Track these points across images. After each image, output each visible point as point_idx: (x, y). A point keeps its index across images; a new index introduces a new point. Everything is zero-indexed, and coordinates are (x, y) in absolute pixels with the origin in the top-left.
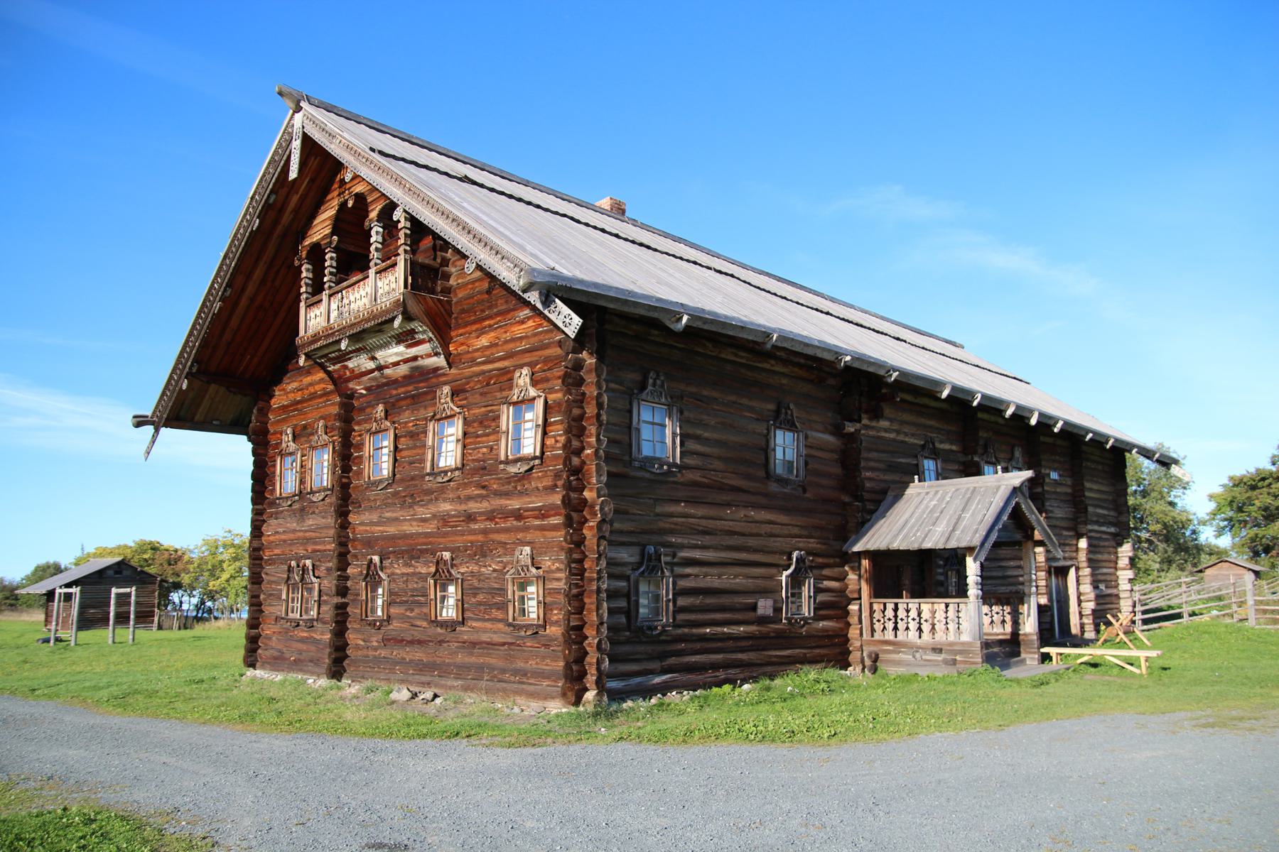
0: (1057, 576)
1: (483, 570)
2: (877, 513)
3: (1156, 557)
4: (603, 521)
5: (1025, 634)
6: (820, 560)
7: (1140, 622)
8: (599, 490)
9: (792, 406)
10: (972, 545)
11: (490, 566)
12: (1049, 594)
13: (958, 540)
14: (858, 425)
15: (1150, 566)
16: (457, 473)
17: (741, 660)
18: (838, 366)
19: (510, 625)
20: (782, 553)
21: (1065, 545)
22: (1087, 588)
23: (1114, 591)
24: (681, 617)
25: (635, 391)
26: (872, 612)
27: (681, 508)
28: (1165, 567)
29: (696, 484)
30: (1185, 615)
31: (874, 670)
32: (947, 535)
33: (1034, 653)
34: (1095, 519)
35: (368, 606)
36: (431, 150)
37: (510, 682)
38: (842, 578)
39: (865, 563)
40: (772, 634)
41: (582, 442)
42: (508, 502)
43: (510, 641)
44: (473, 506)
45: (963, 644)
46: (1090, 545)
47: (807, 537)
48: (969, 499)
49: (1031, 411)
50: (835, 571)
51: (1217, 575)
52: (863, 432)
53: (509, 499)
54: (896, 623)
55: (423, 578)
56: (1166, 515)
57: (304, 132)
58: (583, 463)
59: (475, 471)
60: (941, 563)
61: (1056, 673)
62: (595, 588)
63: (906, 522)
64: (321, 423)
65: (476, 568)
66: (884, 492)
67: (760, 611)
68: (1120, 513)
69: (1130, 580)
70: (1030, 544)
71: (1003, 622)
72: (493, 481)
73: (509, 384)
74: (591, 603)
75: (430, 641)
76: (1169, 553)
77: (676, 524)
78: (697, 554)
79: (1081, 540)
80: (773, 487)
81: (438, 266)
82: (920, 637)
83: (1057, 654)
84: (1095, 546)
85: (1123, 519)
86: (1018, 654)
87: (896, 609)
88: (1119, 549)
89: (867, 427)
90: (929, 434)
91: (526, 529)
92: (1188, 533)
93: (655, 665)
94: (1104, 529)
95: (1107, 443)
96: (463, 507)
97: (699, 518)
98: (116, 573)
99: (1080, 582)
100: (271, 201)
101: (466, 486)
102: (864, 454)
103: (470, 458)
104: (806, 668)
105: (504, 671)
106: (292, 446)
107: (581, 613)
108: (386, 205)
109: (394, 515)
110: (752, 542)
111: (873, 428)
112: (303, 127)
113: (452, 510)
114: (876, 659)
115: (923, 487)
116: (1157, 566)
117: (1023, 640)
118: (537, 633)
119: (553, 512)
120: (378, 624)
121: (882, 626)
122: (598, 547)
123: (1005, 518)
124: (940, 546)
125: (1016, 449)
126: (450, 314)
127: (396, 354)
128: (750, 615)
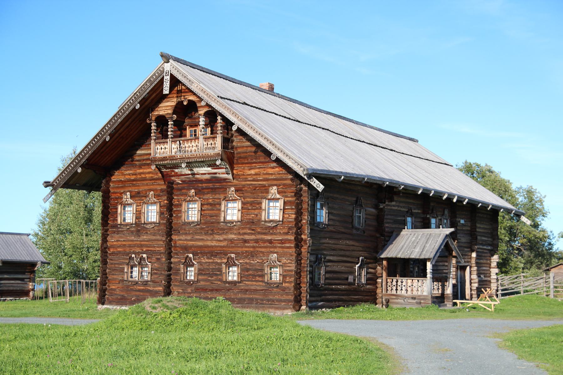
0: (461, 270)
1: (252, 262)
2: (390, 241)
3: (522, 259)
4: (309, 246)
5: (447, 294)
6: (368, 261)
7: (500, 295)
8: (308, 235)
9: (361, 199)
10: (430, 257)
11: (256, 261)
12: (457, 279)
13: (425, 255)
14: (384, 205)
15: (518, 265)
16: (239, 223)
17: (342, 299)
18: (383, 186)
19: (265, 283)
20: (356, 258)
21: (465, 255)
22: (474, 277)
23: (488, 279)
24: (327, 281)
26: (387, 282)
27: (327, 240)
28: (528, 266)
29: (331, 231)
30: (522, 292)
31: (387, 306)
32: (420, 253)
33: (450, 302)
34: (481, 242)
36: (210, 74)
37: (266, 304)
38: (375, 268)
39: (385, 263)
40: (352, 290)
41: (301, 218)
42: (265, 237)
43: (266, 289)
44: (247, 237)
45: (424, 296)
46: (477, 255)
47: (364, 251)
48: (429, 238)
49: (454, 196)
50: (374, 265)
51: (558, 273)
52: (386, 207)
53: (266, 236)
55: (220, 264)
56: (530, 233)
57: (171, 73)
58: (302, 225)
59: (248, 223)
60: (412, 263)
61: (459, 309)
62: (306, 270)
63: (403, 246)
65: (248, 261)
66: (392, 232)
67: (349, 280)
68: (494, 239)
69: (497, 274)
70: (451, 257)
71: (438, 289)
72: (258, 228)
73: (268, 192)
74: (304, 275)
75: (223, 290)
76: (532, 257)
77: (326, 247)
78: (331, 258)
79: (473, 253)
80: (354, 231)
81: (230, 137)
82: (407, 293)
83: (460, 303)
84: (480, 256)
85: (495, 242)
86: (444, 302)
87: (397, 282)
88: (492, 258)
89: (387, 205)
90: (410, 206)
91: (275, 247)
92: (546, 244)
93: (319, 299)
94: (485, 247)
95: (488, 207)
96: (242, 237)
97: (331, 244)
99: (472, 273)
101: (243, 228)
103: (245, 218)
104: (363, 304)
105: (262, 300)
106: (130, 201)
107: (300, 279)
108: (210, 110)
109: (201, 237)
110: (348, 253)
113: (236, 238)
114: (388, 302)
115: (409, 232)
116: (522, 265)
117: (446, 296)
118: (278, 286)
119: (287, 242)
120: (192, 283)
121: (391, 288)
122: (307, 255)
123: (442, 247)
124: (417, 257)
125: (446, 210)
126: (234, 157)
127: (205, 170)
128: (345, 282)
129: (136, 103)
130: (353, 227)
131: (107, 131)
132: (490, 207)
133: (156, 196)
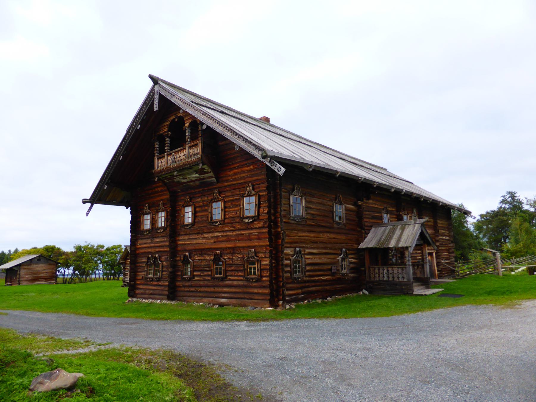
6: (351, 252)
25: (291, 192)
35: (184, 273)
49: (422, 197)
54: (379, 274)
57: (159, 93)
64: (161, 202)
89: (365, 203)
98: (38, 260)
100: (144, 118)
102: (364, 213)
111: (367, 203)
112: (159, 91)
125: (414, 209)
127: (195, 177)
129: (138, 124)
130: (334, 221)
131: (120, 152)
132: (423, 220)
133: (164, 205)
